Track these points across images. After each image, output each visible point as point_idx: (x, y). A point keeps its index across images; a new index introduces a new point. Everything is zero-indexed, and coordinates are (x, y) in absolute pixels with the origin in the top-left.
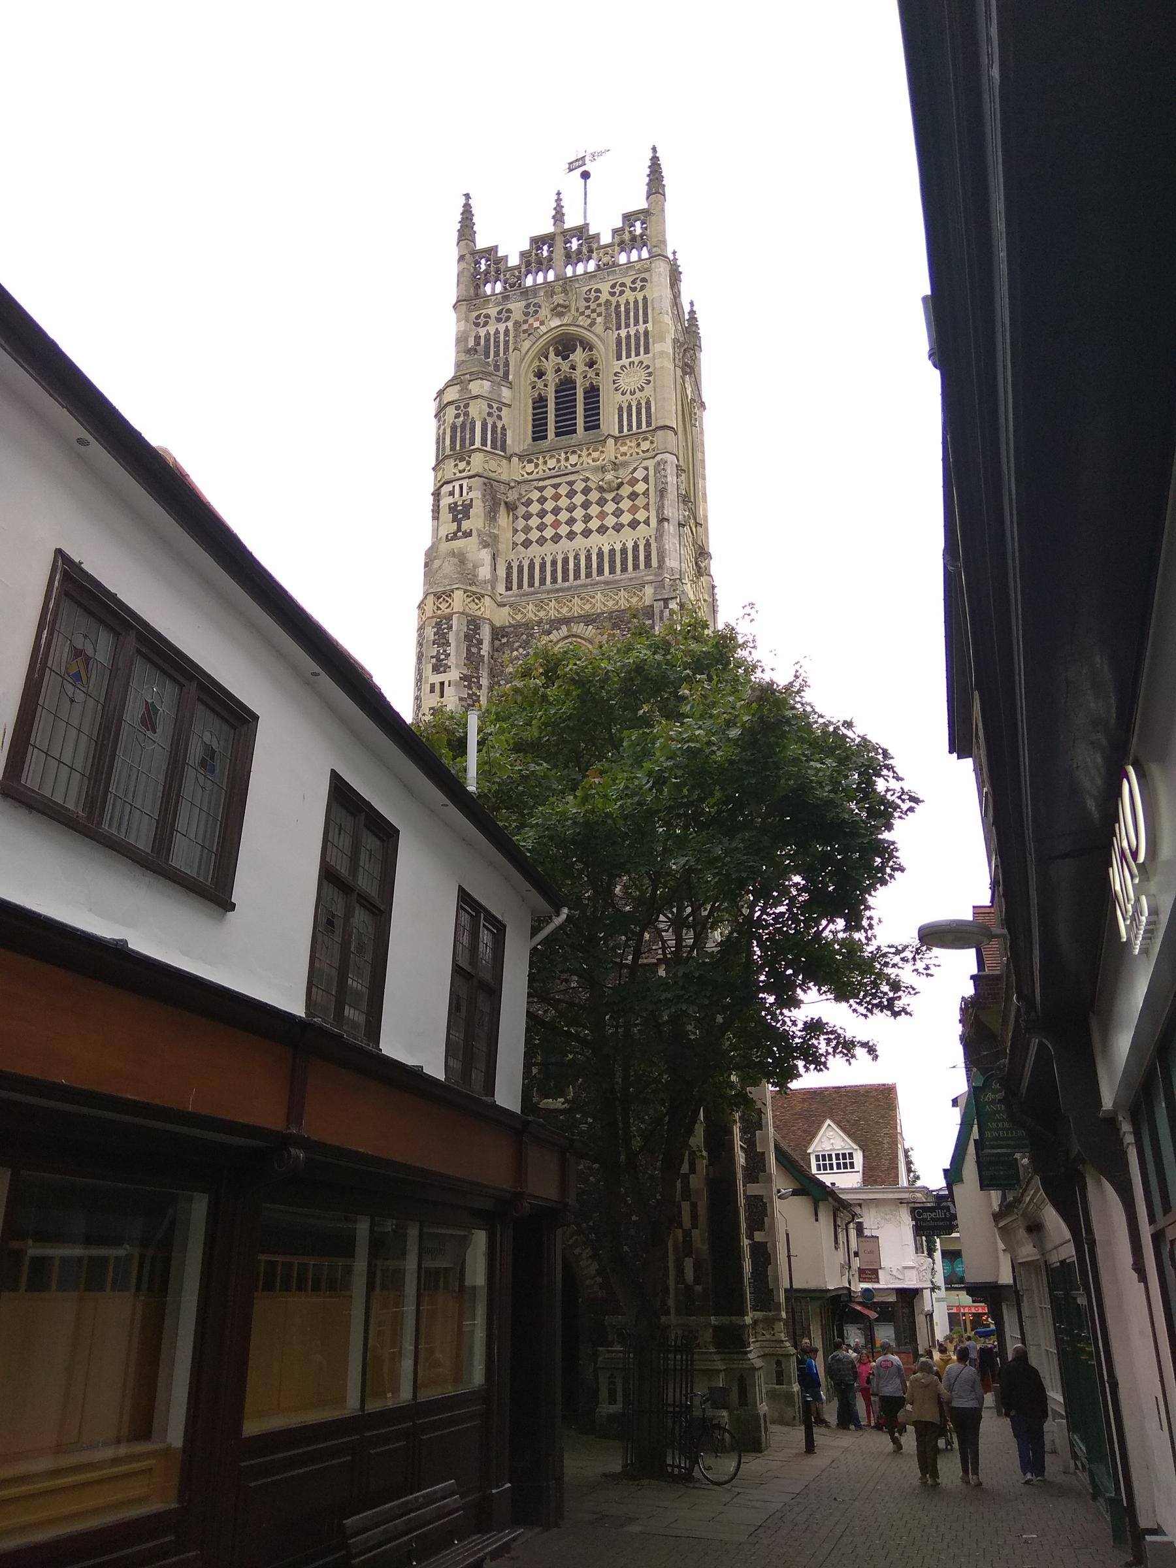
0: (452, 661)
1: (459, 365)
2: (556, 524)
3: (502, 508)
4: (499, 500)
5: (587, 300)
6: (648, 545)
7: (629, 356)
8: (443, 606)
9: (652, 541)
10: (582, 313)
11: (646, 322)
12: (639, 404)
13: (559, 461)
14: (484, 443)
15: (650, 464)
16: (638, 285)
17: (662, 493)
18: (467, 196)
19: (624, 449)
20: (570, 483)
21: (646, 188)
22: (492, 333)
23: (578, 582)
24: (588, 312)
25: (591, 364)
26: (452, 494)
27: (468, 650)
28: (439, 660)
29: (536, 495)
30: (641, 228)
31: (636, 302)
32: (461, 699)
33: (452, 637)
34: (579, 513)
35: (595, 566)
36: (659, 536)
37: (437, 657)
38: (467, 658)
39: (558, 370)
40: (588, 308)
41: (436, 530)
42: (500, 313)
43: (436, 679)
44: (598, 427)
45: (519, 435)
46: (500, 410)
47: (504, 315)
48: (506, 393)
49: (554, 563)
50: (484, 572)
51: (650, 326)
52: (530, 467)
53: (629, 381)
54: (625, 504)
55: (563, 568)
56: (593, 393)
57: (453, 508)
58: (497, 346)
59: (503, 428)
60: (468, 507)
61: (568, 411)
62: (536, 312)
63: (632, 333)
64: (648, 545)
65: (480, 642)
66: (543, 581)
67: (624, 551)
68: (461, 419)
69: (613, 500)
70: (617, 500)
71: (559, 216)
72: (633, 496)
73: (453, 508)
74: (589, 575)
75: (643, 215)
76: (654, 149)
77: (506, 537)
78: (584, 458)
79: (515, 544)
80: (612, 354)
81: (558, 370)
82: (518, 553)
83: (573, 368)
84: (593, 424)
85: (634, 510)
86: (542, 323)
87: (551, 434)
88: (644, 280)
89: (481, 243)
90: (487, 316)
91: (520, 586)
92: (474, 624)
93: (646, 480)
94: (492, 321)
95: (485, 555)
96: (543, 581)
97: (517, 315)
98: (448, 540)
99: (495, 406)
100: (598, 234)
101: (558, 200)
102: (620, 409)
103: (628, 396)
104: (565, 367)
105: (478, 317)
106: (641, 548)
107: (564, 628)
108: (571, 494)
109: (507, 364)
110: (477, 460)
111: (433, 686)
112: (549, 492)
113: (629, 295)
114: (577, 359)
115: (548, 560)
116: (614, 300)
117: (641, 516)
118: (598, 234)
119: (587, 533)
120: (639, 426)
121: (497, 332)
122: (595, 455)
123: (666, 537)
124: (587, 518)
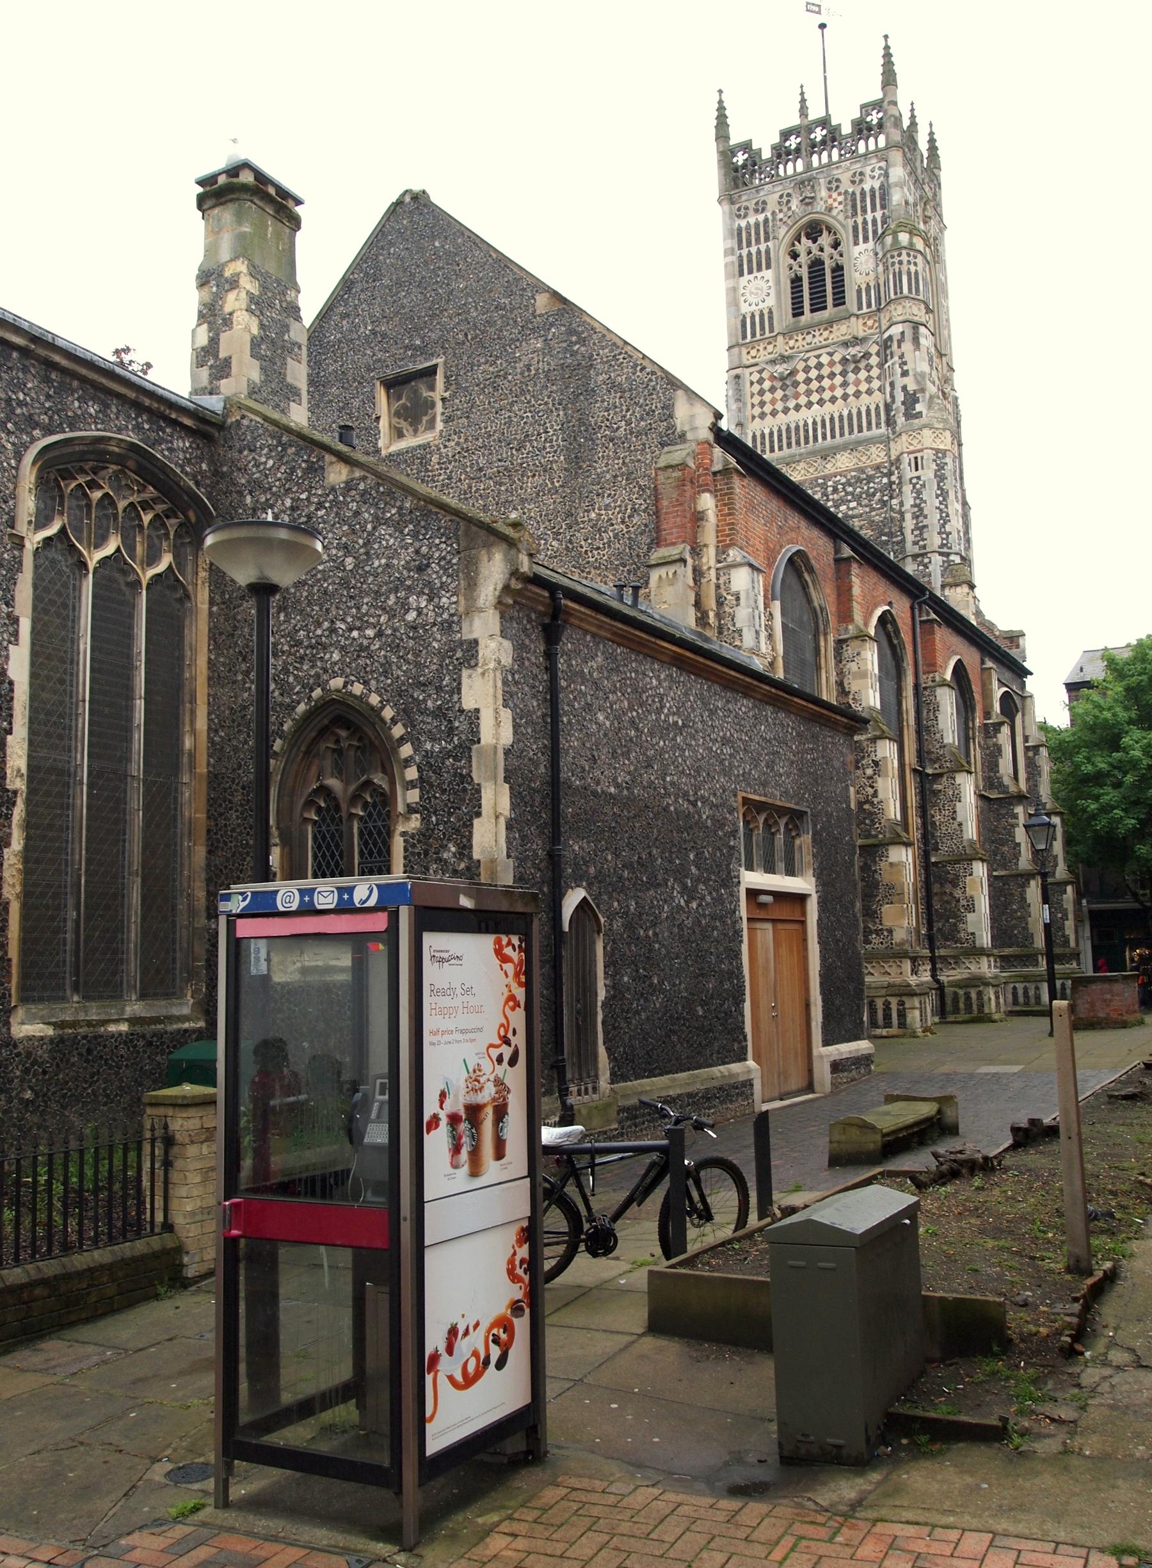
21: (714, 130)
25: (836, 245)
30: (880, 121)
44: (844, 303)
46: (915, 257)
49: (771, 434)
56: (838, 269)
71: (803, 111)
75: (877, 105)
78: (762, 352)
81: (809, 253)
83: (822, 250)
84: (839, 300)
89: (735, 139)
94: (751, 212)
99: (891, 260)
100: (760, 149)
101: (802, 94)
104: (815, 251)
112: (812, 362)
114: (824, 243)
118: (760, 149)
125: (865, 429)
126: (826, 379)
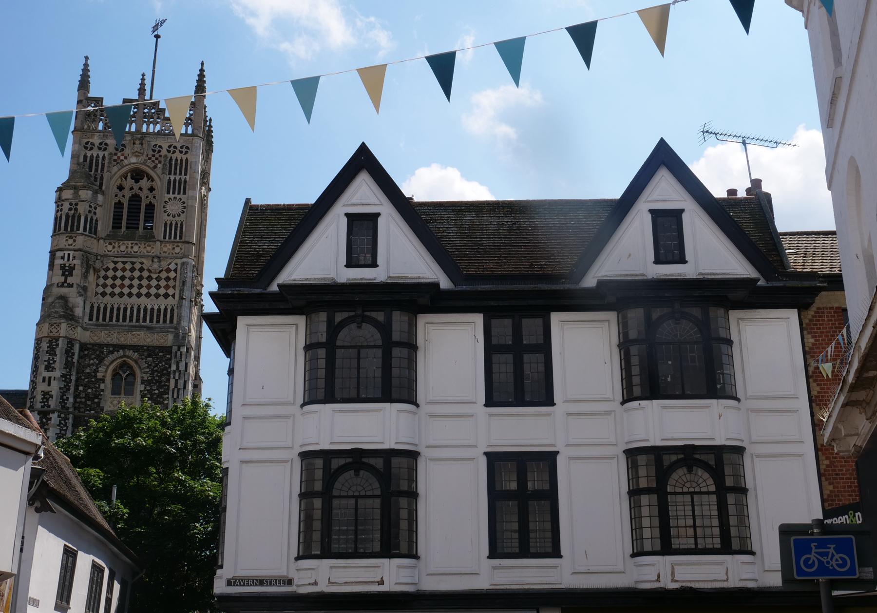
0: (57, 365)
1: (72, 173)
2: (122, 286)
3: (92, 272)
4: (89, 262)
5: (154, 151)
6: (172, 310)
7: (174, 193)
8: (54, 331)
9: (175, 308)
10: (150, 159)
11: (186, 174)
12: (176, 224)
13: (127, 247)
14: (85, 230)
15: (179, 262)
16: (184, 150)
17: (184, 283)
18: (87, 58)
19: (165, 249)
20: (133, 263)
22: (95, 156)
23: (131, 324)
24: (153, 159)
26: (63, 258)
27: (67, 359)
28: (49, 363)
29: (112, 266)
31: (181, 160)
32: (60, 388)
33: (58, 351)
34: (136, 282)
35: (142, 316)
36: (180, 306)
37: (48, 361)
38: (66, 364)
39: (132, 189)
40: (154, 156)
41: (49, 278)
42: (101, 144)
43: (47, 374)
45: (104, 226)
46: (95, 208)
47: (103, 146)
48: (100, 197)
50: (78, 311)
51: (188, 177)
52: (110, 248)
53: (174, 208)
54: (163, 283)
55: (123, 314)
56: (150, 207)
57: (63, 267)
58: (97, 165)
59: (97, 220)
60: (72, 268)
61: (134, 217)
62: (123, 150)
63: (178, 179)
64: (172, 310)
65: (73, 354)
66: (111, 319)
67: (159, 310)
68: (73, 212)
69: (156, 279)
70: (158, 279)
71: (142, 91)
72: (168, 279)
73: (63, 267)
74: (138, 321)
76: (202, 64)
77: (92, 288)
78: (142, 249)
79: (97, 294)
80: (165, 191)
82: (98, 299)
85: (167, 287)
86: (126, 158)
87: (123, 229)
88: (187, 148)
89: (92, 94)
90: (93, 144)
91: (98, 319)
92: (71, 342)
93: (175, 271)
94: (96, 148)
95: (80, 300)
96: (111, 319)
97: (111, 149)
98: (58, 286)
102: (166, 224)
103: (171, 218)
105: (87, 143)
106: (169, 311)
107: (121, 351)
108: (132, 270)
109: (102, 178)
110: (80, 239)
111: (44, 379)
112: (120, 266)
113: (178, 155)
115: (116, 306)
116: (169, 155)
117: (171, 291)
119: (139, 295)
120: (175, 238)
121: (98, 156)
122: (149, 249)
123: (183, 308)
124: (140, 286)
125: (134, 320)
126: (145, 280)
